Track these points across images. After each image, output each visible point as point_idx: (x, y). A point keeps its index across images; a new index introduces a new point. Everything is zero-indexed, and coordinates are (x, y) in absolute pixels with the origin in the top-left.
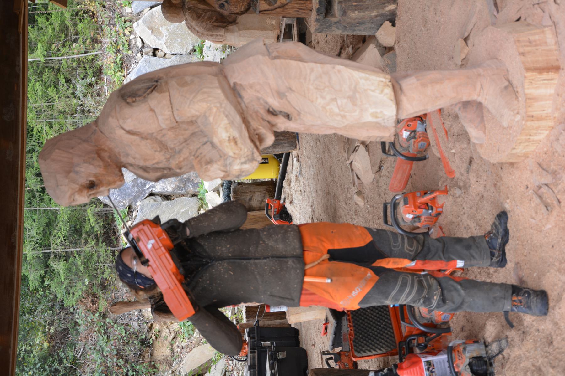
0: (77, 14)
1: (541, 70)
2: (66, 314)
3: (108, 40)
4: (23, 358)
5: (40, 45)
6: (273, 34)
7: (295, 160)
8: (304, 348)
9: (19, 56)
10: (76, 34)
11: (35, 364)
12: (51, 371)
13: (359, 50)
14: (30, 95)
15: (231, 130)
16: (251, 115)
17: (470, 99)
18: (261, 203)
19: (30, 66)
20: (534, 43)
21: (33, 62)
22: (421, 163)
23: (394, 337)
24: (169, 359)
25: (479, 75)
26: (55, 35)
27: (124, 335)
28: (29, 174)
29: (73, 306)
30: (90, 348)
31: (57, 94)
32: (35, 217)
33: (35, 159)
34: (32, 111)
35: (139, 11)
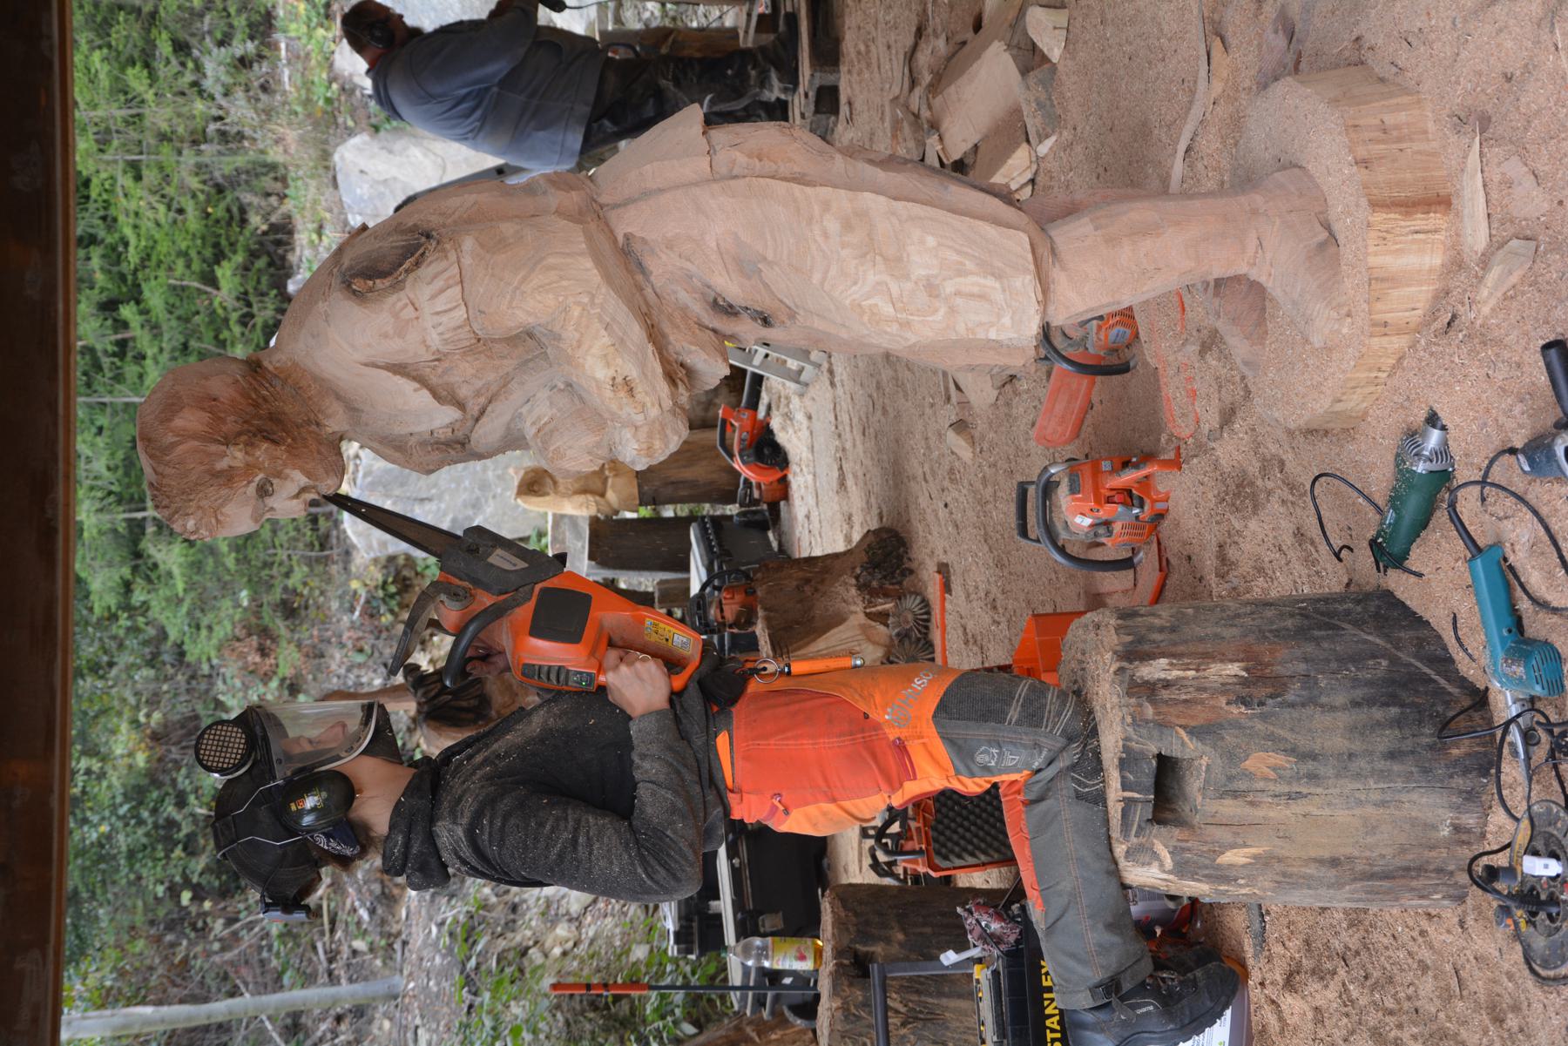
1: (1408, 206)
4: (84, 792)
12: (156, 826)
13: (967, 49)
14: (80, 92)
15: (619, 361)
16: (670, 317)
17: (1230, 273)
18: (706, 409)
20: (1395, 133)
22: (1116, 379)
25: (1255, 212)
29: (209, 659)
31: (151, 86)
32: (103, 420)
33: (96, 262)
34: (84, 130)
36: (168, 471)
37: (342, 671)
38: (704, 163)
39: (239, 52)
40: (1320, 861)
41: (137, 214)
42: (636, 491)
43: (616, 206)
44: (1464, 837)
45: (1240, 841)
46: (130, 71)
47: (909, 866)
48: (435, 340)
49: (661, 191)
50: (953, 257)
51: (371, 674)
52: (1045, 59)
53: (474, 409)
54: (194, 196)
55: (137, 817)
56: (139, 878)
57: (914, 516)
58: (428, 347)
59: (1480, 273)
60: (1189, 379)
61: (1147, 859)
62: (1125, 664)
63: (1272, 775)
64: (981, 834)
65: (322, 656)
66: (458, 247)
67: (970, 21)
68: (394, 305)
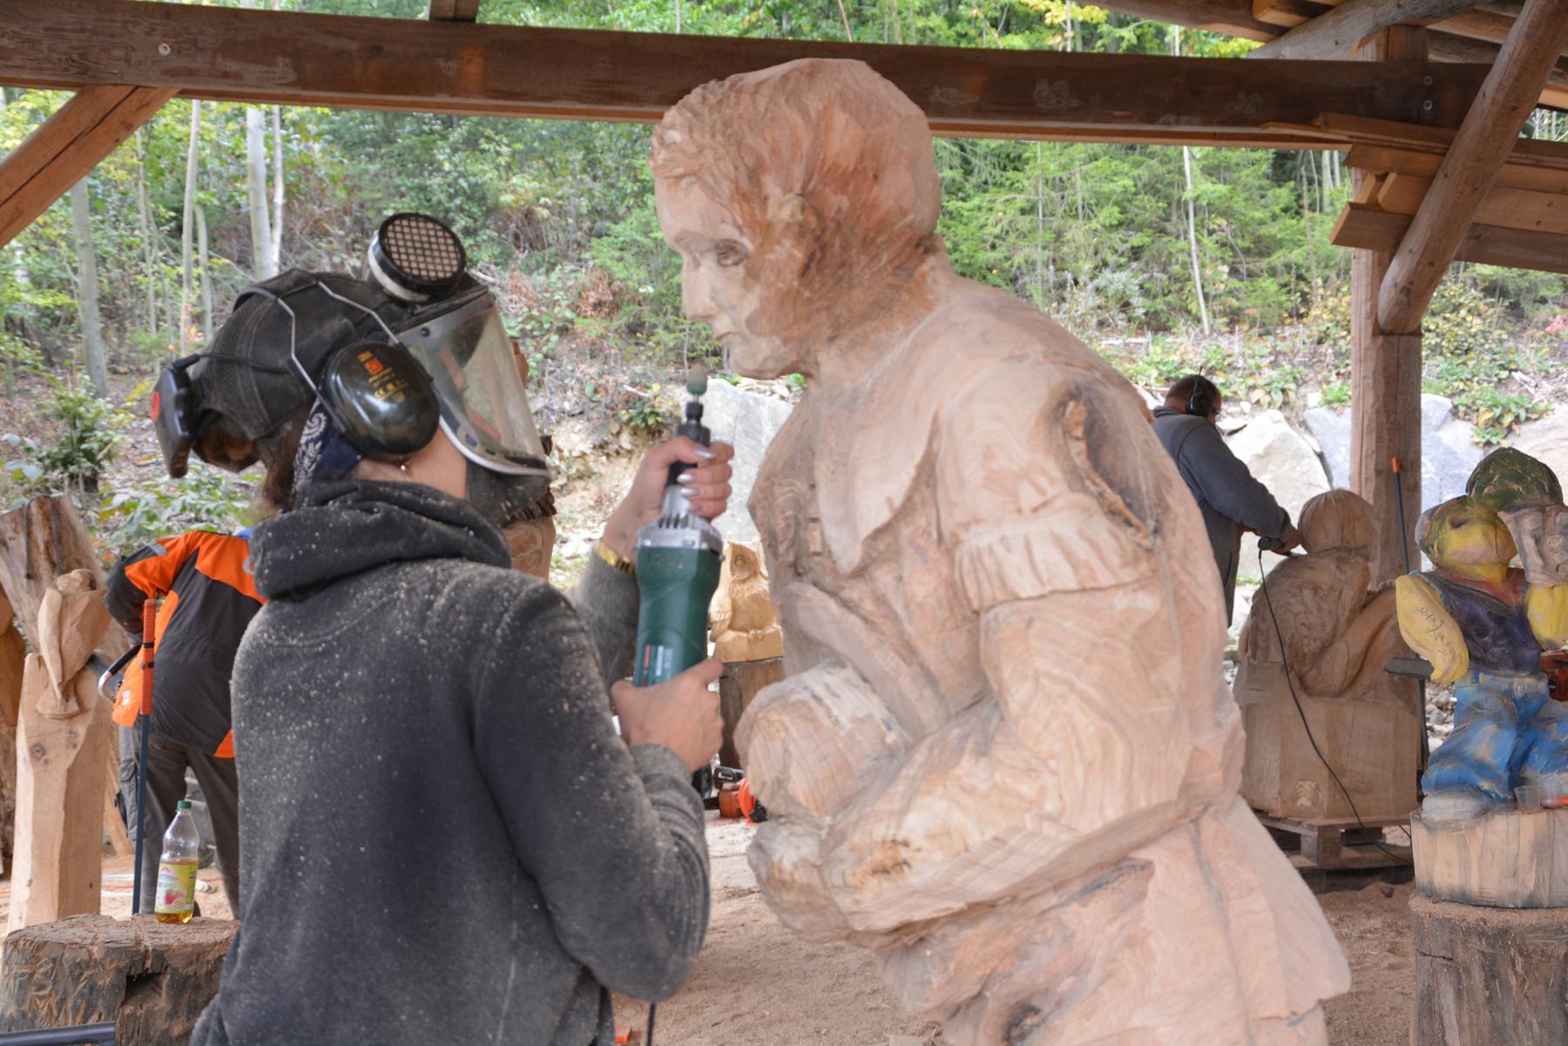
4: (483, 151)
5: (1222, 189)
9: (1205, 124)
12: (447, 211)
26: (1247, 224)
31: (1104, 226)
35: (1311, 423)
36: (762, 102)
37: (578, 374)
38: (1277, 1007)
41: (991, 210)
42: (734, 660)
46: (1116, 210)
48: (979, 539)
51: (574, 400)
53: (854, 592)
54: (1007, 259)
55: (456, 195)
56: (402, 195)
57: (696, 998)
58: (966, 526)
65: (592, 357)
66: (1142, 584)
68: (1043, 472)
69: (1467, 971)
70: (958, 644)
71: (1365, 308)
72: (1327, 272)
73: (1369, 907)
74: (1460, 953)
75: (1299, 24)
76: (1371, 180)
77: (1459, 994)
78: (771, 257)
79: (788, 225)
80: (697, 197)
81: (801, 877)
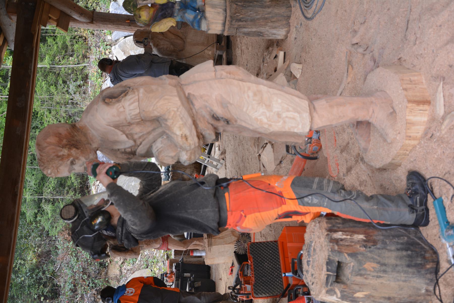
0: (74, 38)
2: (50, 241)
3: (94, 57)
4: (19, 269)
5: (47, 57)
6: (211, 62)
7: (217, 148)
8: (213, 280)
9: (32, 62)
10: (73, 51)
11: (26, 273)
12: (36, 279)
13: (272, 76)
14: (37, 89)
19: (39, 70)
20: (414, 82)
21: (41, 68)
23: (283, 285)
24: (118, 277)
25: (372, 102)
26: (58, 51)
27: (88, 258)
28: (32, 144)
29: (55, 236)
30: (65, 266)
31: (56, 90)
32: (34, 173)
35: (116, 38)
36: (44, 155)
38: (213, 74)
39: (78, 84)
40: (385, 298)
41: (49, 122)
43: (185, 85)
44: (429, 293)
45: (361, 290)
47: (241, 298)
49: (199, 81)
50: (286, 106)
52: (295, 77)
53: (138, 143)
54: (64, 118)
56: (31, 293)
58: (126, 121)
59: (442, 122)
60: (336, 160)
61: (333, 294)
62: (329, 233)
63: (372, 270)
64: (267, 288)
66: (138, 91)
67: (273, 69)
69: (239, 25)
70: (148, 124)
71: (85, 25)
72: (73, 30)
73: (235, 40)
74: (236, 26)
75: (4, 34)
76: (50, 20)
77: (244, 28)
78: (74, 155)
79: (68, 151)
80: (62, 168)
81: (189, 154)
